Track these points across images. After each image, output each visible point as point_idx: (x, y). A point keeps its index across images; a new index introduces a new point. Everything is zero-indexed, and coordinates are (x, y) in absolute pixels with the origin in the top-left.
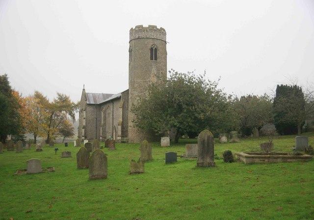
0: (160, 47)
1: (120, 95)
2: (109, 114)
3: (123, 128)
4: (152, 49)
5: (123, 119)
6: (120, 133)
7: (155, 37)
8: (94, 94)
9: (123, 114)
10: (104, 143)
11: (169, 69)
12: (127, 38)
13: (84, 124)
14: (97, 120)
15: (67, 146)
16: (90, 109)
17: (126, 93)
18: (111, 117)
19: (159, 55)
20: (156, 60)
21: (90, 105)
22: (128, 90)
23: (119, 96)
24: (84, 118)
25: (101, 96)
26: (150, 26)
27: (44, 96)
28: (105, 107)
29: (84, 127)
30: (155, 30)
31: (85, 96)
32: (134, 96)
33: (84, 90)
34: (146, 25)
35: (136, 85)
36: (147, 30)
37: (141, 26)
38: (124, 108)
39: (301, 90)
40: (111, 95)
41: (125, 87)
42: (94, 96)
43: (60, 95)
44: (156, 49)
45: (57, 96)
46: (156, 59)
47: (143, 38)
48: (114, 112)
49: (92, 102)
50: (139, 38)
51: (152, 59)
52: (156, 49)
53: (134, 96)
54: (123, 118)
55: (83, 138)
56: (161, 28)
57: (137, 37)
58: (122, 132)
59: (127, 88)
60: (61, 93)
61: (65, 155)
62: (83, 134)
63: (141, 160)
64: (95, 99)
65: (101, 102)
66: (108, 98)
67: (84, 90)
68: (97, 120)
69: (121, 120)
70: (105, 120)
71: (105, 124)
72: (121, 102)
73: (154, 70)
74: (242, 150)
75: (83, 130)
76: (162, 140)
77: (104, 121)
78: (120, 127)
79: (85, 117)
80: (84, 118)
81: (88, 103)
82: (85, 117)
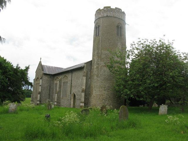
1: (84, 65)
2: (65, 83)
5: (86, 87)
6: (83, 100)
9: (86, 82)
11: (128, 48)
12: (93, 18)
13: (40, 90)
14: (50, 89)
16: (45, 78)
17: (90, 63)
20: (121, 36)
22: (92, 61)
23: (82, 66)
24: (40, 86)
28: (60, 77)
29: (40, 93)
31: (41, 67)
33: (40, 62)
34: (113, 7)
35: (103, 56)
36: (114, 11)
37: (110, 7)
38: (89, 78)
41: (89, 58)
42: (49, 68)
45: (16, 65)
48: (73, 81)
50: (107, 16)
51: (118, 34)
57: (105, 15)
62: (38, 99)
67: (40, 62)
68: (50, 89)
69: (84, 87)
71: (60, 91)
74: (15, 112)
75: (39, 95)
79: (41, 84)
80: (40, 86)
82: (41, 84)
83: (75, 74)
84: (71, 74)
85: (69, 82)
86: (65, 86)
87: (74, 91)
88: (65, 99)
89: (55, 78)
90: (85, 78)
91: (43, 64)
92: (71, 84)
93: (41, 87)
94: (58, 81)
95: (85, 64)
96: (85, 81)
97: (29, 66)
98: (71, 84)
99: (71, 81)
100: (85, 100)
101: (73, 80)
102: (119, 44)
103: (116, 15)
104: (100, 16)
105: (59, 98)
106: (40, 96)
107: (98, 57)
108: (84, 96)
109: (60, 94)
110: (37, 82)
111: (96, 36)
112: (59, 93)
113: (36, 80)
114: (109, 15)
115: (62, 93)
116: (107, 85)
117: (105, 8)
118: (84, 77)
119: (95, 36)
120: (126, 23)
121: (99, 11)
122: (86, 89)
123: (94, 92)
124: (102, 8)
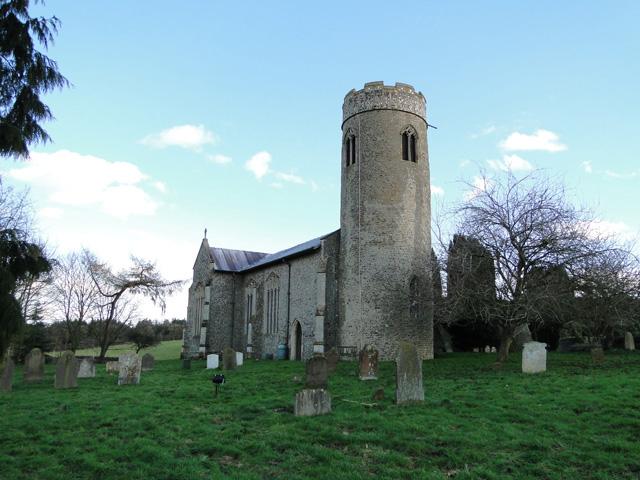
0: (420, 133)
4: (405, 136)
6: (320, 336)
7: (410, 109)
8: (229, 251)
14: (235, 307)
16: (218, 281)
19: (419, 151)
22: (339, 231)
23: (315, 245)
24: (207, 303)
25: (243, 258)
26: (398, 85)
28: (259, 278)
30: (410, 94)
32: (363, 242)
33: (205, 240)
38: (335, 274)
39: (41, 250)
40: (259, 256)
42: (228, 254)
44: (412, 136)
46: (414, 159)
49: (226, 268)
51: (406, 158)
52: (412, 136)
53: (363, 242)
55: (203, 349)
57: (369, 106)
58: (327, 333)
59: (335, 226)
60: (92, 252)
62: (203, 340)
63: (607, 253)
65: (244, 268)
66: (256, 260)
67: (205, 240)
68: (235, 307)
70: (260, 306)
71: (260, 316)
72: (322, 257)
78: (320, 321)
80: (207, 303)
81: (216, 268)
85: (283, 292)
89: (249, 278)
91: (212, 244)
92: (289, 294)
93: (207, 307)
95: (321, 239)
98: (289, 294)
104: (356, 110)
105: (257, 334)
107: (356, 218)
108: (322, 325)
109: (261, 325)
111: (348, 164)
114: (379, 105)
117: (366, 86)
119: (345, 165)
121: (352, 98)
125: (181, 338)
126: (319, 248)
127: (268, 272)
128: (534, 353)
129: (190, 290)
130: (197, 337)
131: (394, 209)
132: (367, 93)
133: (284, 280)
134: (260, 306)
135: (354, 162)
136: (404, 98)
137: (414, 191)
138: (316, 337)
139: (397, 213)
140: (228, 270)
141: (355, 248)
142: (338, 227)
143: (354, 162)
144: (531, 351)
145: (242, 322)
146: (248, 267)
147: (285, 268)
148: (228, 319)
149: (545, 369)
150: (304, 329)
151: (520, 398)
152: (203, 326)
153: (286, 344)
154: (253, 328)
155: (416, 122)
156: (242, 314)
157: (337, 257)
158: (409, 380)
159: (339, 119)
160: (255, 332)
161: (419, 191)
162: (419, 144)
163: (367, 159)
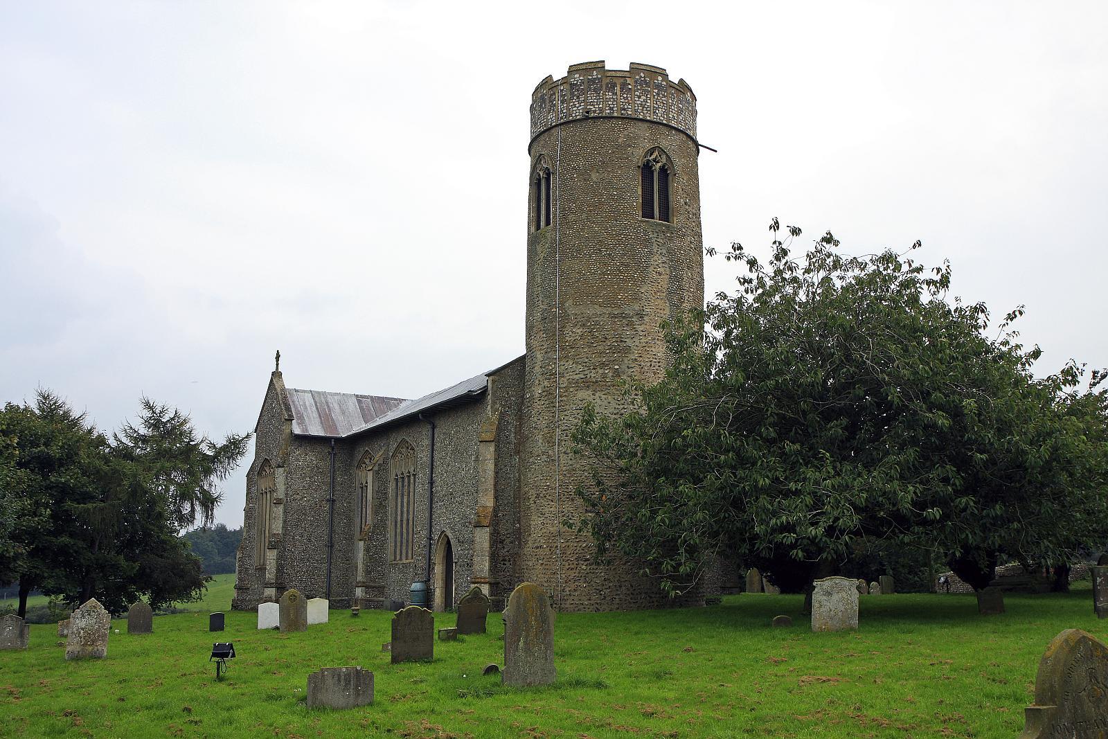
0: (678, 162)
2: (405, 480)
3: (496, 541)
4: (647, 169)
6: (483, 565)
7: (660, 116)
9: (496, 473)
10: (455, 617)
13: (278, 527)
15: (222, 629)
16: (304, 459)
18: (421, 488)
19: (677, 198)
21: (306, 440)
23: (476, 387)
24: (279, 502)
26: (635, 68)
27: (75, 414)
28: (379, 452)
30: (658, 86)
32: (564, 382)
33: (277, 375)
34: (617, 62)
35: (574, 333)
36: (624, 85)
37: (599, 66)
40: (385, 403)
42: (322, 402)
43: (148, 406)
44: (663, 170)
46: (666, 215)
47: (611, 118)
48: (438, 470)
49: (316, 430)
51: (648, 213)
54: (496, 491)
56: (681, 80)
57: (577, 113)
58: (496, 560)
61: (334, 695)
62: (270, 575)
64: (325, 417)
67: (277, 375)
69: (488, 501)
70: (380, 506)
71: (380, 527)
72: (490, 412)
73: (658, 263)
75: (271, 556)
76: (817, 596)
77: (376, 513)
78: (483, 538)
79: (281, 493)
80: (279, 502)
82: (281, 493)
83: (447, 428)
84: (429, 427)
85: (423, 477)
86: (405, 500)
87: (445, 521)
88: (405, 566)
89: (361, 450)
90: (489, 452)
91: (289, 382)
92: (432, 483)
93: (281, 508)
94: (370, 474)
95: (488, 375)
96: (490, 466)
97: (148, 406)
98: (432, 483)
99: (428, 471)
100: (494, 568)
101: (437, 463)
102: (657, 259)
103: (640, 103)
104: (552, 119)
105: (374, 560)
106: (280, 557)
107: (551, 334)
108: (486, 545)
109: (383, 543)
110: (264, 484)
111: (538, 227)
112: (374, 536)
113: (259, 474)
114: (595, 109)
115: (390, 535)
116: (214, 478)
117: (573, 70)
118: (482, 447)
119: (533, 229)
120: (697, 145)
121: (546, 93)
122: (496, 510)
123: (536, 521)
124: (559, 73)
125: (232, 571)
126: (484, 391)
127: (393, 441)
128: (835, 597)
129: (249, 476)
130: (262, 569)
131: (623, 316)
132: (572, 85)
133: (424, 456)
134: (380, 506)
135: (548, 223)
136: (646, 92)
137: (664, 282)
138: (476, 567)
139: (630, 324)
140: (322, 434)
141: (548, 393)
142: (522, 351)
143: (548, 223)
144: (829, 594)
145: (350, 539)
146: (361, 426)
147: (425, 430)
148: (323, 531)
149: (326, 619)
150: (456, 550)
151: (1070, 711)
152: (272, 547)
153: (427, 581)
154: (367, 550)
155: (670, 142)
156: (350, 523)
157: (520, 410)
158: (527, 649)
159: (524, 135)
160: (371, 558)
161: (676, 279)
162: (677, 187)
163: (571, 217)
